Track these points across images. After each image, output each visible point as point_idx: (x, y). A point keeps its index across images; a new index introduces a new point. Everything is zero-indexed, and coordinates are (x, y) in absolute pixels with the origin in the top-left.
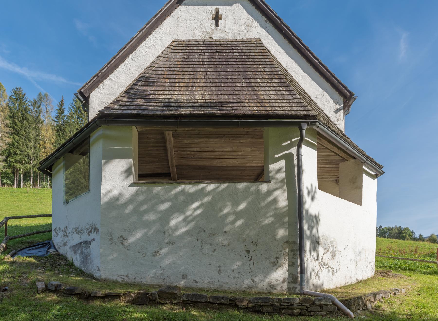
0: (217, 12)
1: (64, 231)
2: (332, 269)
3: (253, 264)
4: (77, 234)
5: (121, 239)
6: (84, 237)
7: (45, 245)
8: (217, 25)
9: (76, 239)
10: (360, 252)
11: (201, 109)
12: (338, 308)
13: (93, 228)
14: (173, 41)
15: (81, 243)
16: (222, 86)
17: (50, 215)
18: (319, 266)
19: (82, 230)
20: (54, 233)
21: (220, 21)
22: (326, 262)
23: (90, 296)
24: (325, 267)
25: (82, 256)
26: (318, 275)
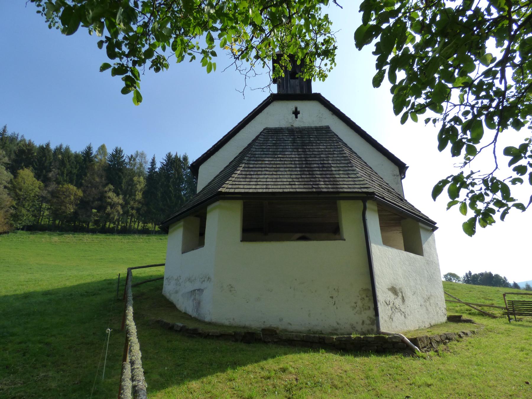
0: (296, 109)
1: (177, 280)
2: (403, 312)
3: (337, 308)
4: (190, 283)
5: (230, 287)
6: (197, 286)
7: (470, 304)
8: (296, 117)
9: (190, 287)
10: (429, 298)
11: (274, 160)
12: (406, 345)
13: (206, 278)
14: (264, 129)
15: (195, 290)
16: (304, 166)
17: (164, 265)
18: (392, 310)
19: (195, 279)
20: (165, 282)
21: (299, 115)
22: (397, 307)
23: (208, 335)
24: (397, 311)
25: (195, 301)
26: (392, 318)
